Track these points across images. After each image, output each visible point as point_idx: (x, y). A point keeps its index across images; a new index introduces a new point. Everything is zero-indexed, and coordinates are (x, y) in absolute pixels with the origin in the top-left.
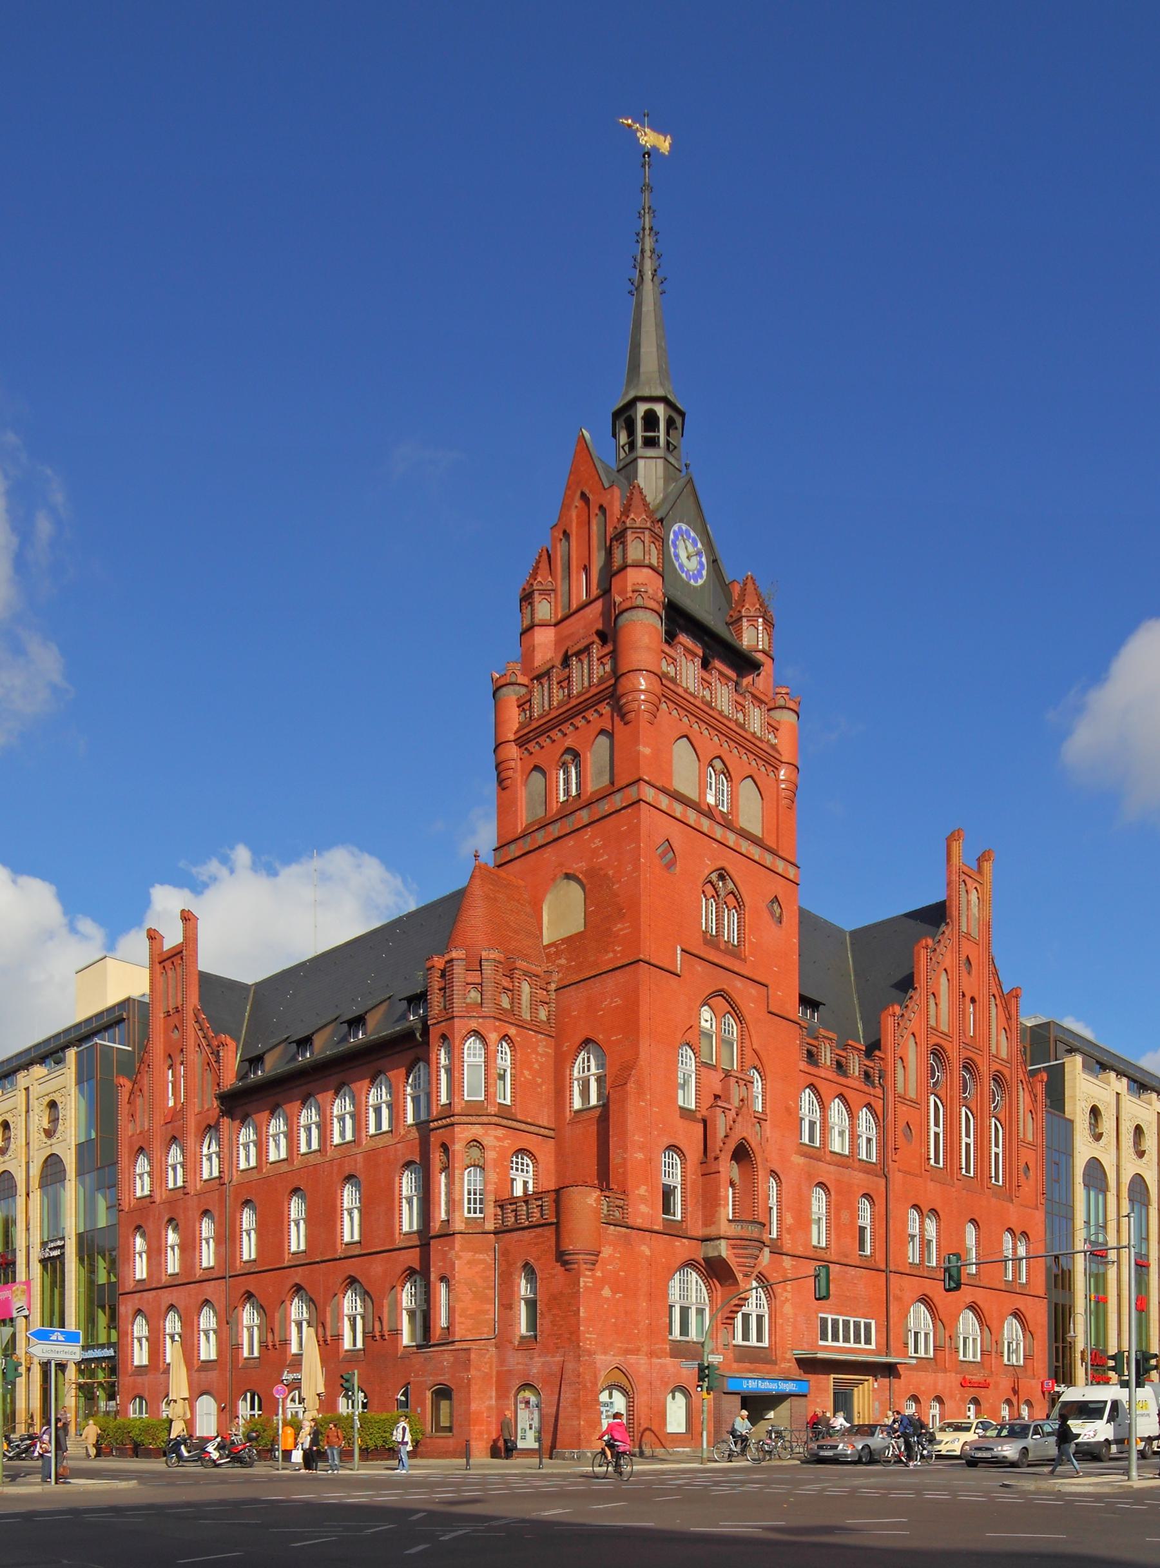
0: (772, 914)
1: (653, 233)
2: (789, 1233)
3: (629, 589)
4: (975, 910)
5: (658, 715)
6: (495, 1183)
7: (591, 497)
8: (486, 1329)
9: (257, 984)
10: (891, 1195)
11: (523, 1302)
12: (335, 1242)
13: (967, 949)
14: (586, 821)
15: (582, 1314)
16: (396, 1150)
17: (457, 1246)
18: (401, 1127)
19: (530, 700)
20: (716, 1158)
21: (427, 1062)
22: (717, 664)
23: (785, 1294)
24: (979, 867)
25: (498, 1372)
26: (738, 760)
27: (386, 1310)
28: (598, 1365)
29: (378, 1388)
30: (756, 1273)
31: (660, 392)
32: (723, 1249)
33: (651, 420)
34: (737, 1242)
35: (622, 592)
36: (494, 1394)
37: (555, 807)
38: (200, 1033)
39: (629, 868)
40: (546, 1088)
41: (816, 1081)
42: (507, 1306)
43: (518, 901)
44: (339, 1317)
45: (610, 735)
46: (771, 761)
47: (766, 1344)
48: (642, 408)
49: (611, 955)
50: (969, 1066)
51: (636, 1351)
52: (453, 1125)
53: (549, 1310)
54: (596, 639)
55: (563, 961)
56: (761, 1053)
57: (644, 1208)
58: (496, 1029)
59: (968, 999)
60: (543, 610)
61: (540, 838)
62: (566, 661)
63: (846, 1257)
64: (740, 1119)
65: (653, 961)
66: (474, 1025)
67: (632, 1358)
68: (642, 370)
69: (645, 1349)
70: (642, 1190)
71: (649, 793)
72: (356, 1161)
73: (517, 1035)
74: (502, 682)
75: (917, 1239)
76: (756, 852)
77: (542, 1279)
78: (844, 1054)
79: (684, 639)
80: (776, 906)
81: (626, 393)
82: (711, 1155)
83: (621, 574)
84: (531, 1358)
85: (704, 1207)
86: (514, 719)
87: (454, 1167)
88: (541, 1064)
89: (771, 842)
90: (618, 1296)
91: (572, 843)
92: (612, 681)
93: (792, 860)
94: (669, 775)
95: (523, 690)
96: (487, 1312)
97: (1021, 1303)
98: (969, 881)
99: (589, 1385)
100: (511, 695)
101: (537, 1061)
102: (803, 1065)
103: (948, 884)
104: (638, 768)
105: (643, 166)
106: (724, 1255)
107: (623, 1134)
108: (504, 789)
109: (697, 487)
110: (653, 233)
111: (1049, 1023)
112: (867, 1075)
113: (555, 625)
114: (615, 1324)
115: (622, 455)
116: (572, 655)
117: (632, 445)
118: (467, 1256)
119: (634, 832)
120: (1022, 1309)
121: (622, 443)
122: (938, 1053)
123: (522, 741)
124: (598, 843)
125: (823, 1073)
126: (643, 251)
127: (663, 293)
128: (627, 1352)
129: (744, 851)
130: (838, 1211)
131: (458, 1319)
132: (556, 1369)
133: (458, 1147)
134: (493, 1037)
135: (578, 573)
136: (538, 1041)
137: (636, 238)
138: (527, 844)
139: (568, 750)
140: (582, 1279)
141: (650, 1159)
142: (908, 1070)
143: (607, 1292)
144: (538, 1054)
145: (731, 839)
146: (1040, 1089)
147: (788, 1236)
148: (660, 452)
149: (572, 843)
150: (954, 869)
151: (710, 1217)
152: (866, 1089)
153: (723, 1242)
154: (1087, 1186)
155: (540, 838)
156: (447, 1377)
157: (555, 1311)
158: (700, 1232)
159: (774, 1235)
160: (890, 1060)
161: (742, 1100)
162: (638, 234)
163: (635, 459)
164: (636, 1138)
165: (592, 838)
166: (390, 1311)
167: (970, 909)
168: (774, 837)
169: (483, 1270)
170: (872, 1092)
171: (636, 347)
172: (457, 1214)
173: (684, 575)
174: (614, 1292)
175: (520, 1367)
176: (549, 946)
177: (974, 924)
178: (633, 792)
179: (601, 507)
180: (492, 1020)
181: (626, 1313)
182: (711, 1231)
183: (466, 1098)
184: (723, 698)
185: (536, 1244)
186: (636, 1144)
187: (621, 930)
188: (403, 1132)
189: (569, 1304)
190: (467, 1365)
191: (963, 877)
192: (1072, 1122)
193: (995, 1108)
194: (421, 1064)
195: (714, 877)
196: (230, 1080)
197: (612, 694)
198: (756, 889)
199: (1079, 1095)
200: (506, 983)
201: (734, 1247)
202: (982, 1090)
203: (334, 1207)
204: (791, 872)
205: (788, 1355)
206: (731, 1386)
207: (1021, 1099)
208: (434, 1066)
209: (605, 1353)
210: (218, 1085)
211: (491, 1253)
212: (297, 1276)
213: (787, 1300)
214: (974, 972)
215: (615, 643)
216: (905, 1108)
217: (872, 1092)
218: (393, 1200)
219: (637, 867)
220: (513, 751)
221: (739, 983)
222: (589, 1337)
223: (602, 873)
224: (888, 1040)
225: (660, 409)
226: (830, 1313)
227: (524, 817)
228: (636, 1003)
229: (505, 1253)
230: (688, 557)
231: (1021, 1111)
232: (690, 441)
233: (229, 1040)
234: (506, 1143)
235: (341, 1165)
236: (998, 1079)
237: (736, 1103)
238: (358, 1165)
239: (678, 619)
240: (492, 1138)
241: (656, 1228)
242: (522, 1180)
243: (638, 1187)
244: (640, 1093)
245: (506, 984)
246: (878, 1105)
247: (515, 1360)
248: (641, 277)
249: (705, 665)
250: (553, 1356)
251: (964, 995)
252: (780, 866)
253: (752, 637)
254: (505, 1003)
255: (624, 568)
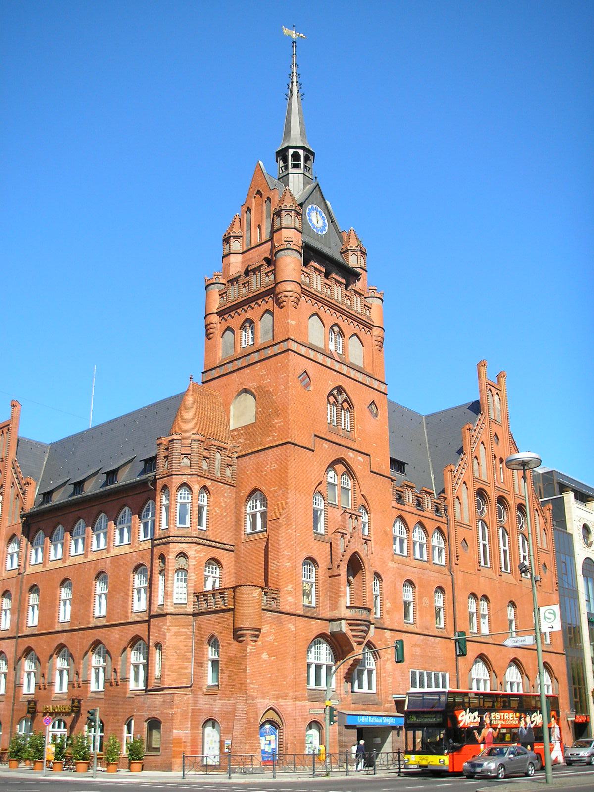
0: (371, 412)
1: (297, 75)
2: (388, 614)
3: (283, 239)
4: (498, 406)
5: (299, 304)
6: (195, 581)
7: (263, 193)
8: (185, 680)
9: (52, 444)
10: (456, 587)
11: (210, 663)
12: (89, 616)
13: (495, 429)
14: (257, 359)
15: (248, 671)
16: (132, 557)
17: (168, 623)
18: (136, 541)
19: (226, 292)
20: (338, 566)
21: (155, 500)
22: (334, 275)
23: (387, 656)
24: (499, 381)
25: (192, 709)
26: (348, 327)
27: (120, 664)
28: (259, 706)
29: (111, 719)
30: (366, 641)
31: (301, 144)
32: (344, 627)
33: (296, 157)
34: (352, 622)
35: (279, 240)
36: (189, 725)
37: (239, 350)
38: (15, 475)
39: (283, 387)
40: (230, 519)
41: (404, 515)
42: (200, 664)
43: (215, 404)
44: (88, 667)
45: (272, 314)
46: (369, 326)
47: (374, 690)
48: (291, 152)
49: (271, 438)
50: (501, 500)
51: (284, 697)
52: (168, 543)
53: (227, 667)
54: (264, 262)
55: (242, 440)
56: (368, 497)
57: (290, 599)
58: (198, 482)
59: (498, 460)
60: (236, 246)
61: (230, 367)
62: (247, 273)
63: (427, 629)
64: (353, 540)
65: (296, 442)
66: (184, 479)
67: (282, 702)
68: (292, 133)
69: (291, 695)
70: (289, 587)
71: (294, 346)
72: (106, 562)
73: (212, 485)
74: (210, 282)
75: (475, 615)
76: (360, 377)
77: (222, 646)
78: (421, 496)
79: (314, 264)
80: (373, 406)
81: (283, 143)
82: (335, 564)
83: (279, 232)
84: (215, 701)
85: (331, 598)
86: (216, 303)
87: (168, 570)
88: (227, 504)
89: (369, 370)
90: (273, 658)
91: (249, 371)
92: (274, 285)
93: (382, 380)
94: (307, 335)
95: (223, 286)
96: (186, 668)
97: (548, 658)
98: (492, 389)
99: (252, 720)
100: (215, 290)
101: (224, 502)
102: (394, 504)
103: (480, 391)
104: (287, 332)
105: (293, 46)
106: (344, 630)
107: (278, 550)
108: (209, 339)
109: (321, 188)
110: (297, 75)
111: (552, 471)
112: (437, 510)
113: (242, 254)
114: (271, 678)
115: (281, 172)
116: (251, 270)
117: (286, 168)
118: (175, 629)
119: (285, 366)
120: (549, 662)
121: (281, 166)
122: (481, 493)
123: (220, 314)
124: (264, 372)
125: (407, 508)
126: (292, 82)
127: (303, 99)
128: (278, 697)
129: (352, 376)
130: (421, 598)
131: (167, 672)
132: (230, 708)
133: (171, 557)
134: (196, 488)
135: (255, 228)
136: (225, 489)
137: (289, 76)
138: (223, 370)
139: (247, 320)
140: (249, 647)
141: (295, 567)
142: (464, 507)
143: (265, 656)
144: (224, 497)
145: (345, 370)
146: (548, 514)
147: (388, 616)
148: (302, 171)
149: (249, 371)
150: (483, 382)
151: (334, 606)
152: (437, 518)
153: (343, 622)
154: (585, 576)
155: (230, 367)
156: (158, 712)
157: (231, 669)
158: (328, 615)
159: (378, 615)
160: (450, 499)
161: (354, 528)
162: (290, 75)
163: (288, 174)
164: (286, 553)
165: (261, 369)
166: (122, 665)
167: (494, 406)
168: (371, 367)
169: (185, 639)
170: (440, 519)
171: (288, 122)
172: (169, 601)
173: (315, 230)
174: (270, 655)
175: (207, 707)
176: (233, 430)
177: (498, 413)
178: (284, 346)
179: (268, 198)
180: (196, 476)
181: (278, 670)
182: (336, 614)
183: (178, 525)
184: (338, 293)
185: (219, 623)
186: (288, 560)
187: (278, 423)
188: (137, 545)
189: (241, 664)
190: (171, 705)
191: (489, 387)
192: (571, 535)
193: (521, 527)
194: (151, 501)
195: (335, 392)
196: (30, 505)
197: (272, 292)
198: (360, 397)
199: (574, 517)
200: (206, 454)
201: (350, 625)
202: (511, 517)
203: (90, 593)
204: (382, 388)
205: (389, 699)
206: (350, 721)
207: (537, 521)
208: (158, 504)
209: (264, 698)
210: (22, 509)
211: (190, 628)
212: (62, 638)
213: (388, 660)
214: (500, 444)
215: (275, 266)
216: (462, 529)
217: (440, 519)
218: (128, 590)
219: (287, 388)
220: (215, 318)
221: (351, 454)
222: (253, 685)
223: (266, 389)
224: (449, 487)
225: (301, 152)
226: (374, 538)
227: (220, 356)
228: (286, 468)
229: (199, 628)
230: (316, 220)
231: (538, 529)
232: (316, 165)
233: (32, 481)
234: (202, 555)
235: (96, 565)
236: (521, 508)
237: (351, 530)
238: (107, 567)
239: (310, 253)
240: (192, 551)
241: (299, 612)
242: (213, 580)
243: (286, 585)
244: (288, 524)
245: (205, 455)
246: (444, 528)
247: (204, 702)
248: (291, 92)
249: (327, 275)
250: (229, 700)
251: (495, 457)
252: (375, 384)
253: (353, 261)
254: (205, 465)
255: (280, 229)
